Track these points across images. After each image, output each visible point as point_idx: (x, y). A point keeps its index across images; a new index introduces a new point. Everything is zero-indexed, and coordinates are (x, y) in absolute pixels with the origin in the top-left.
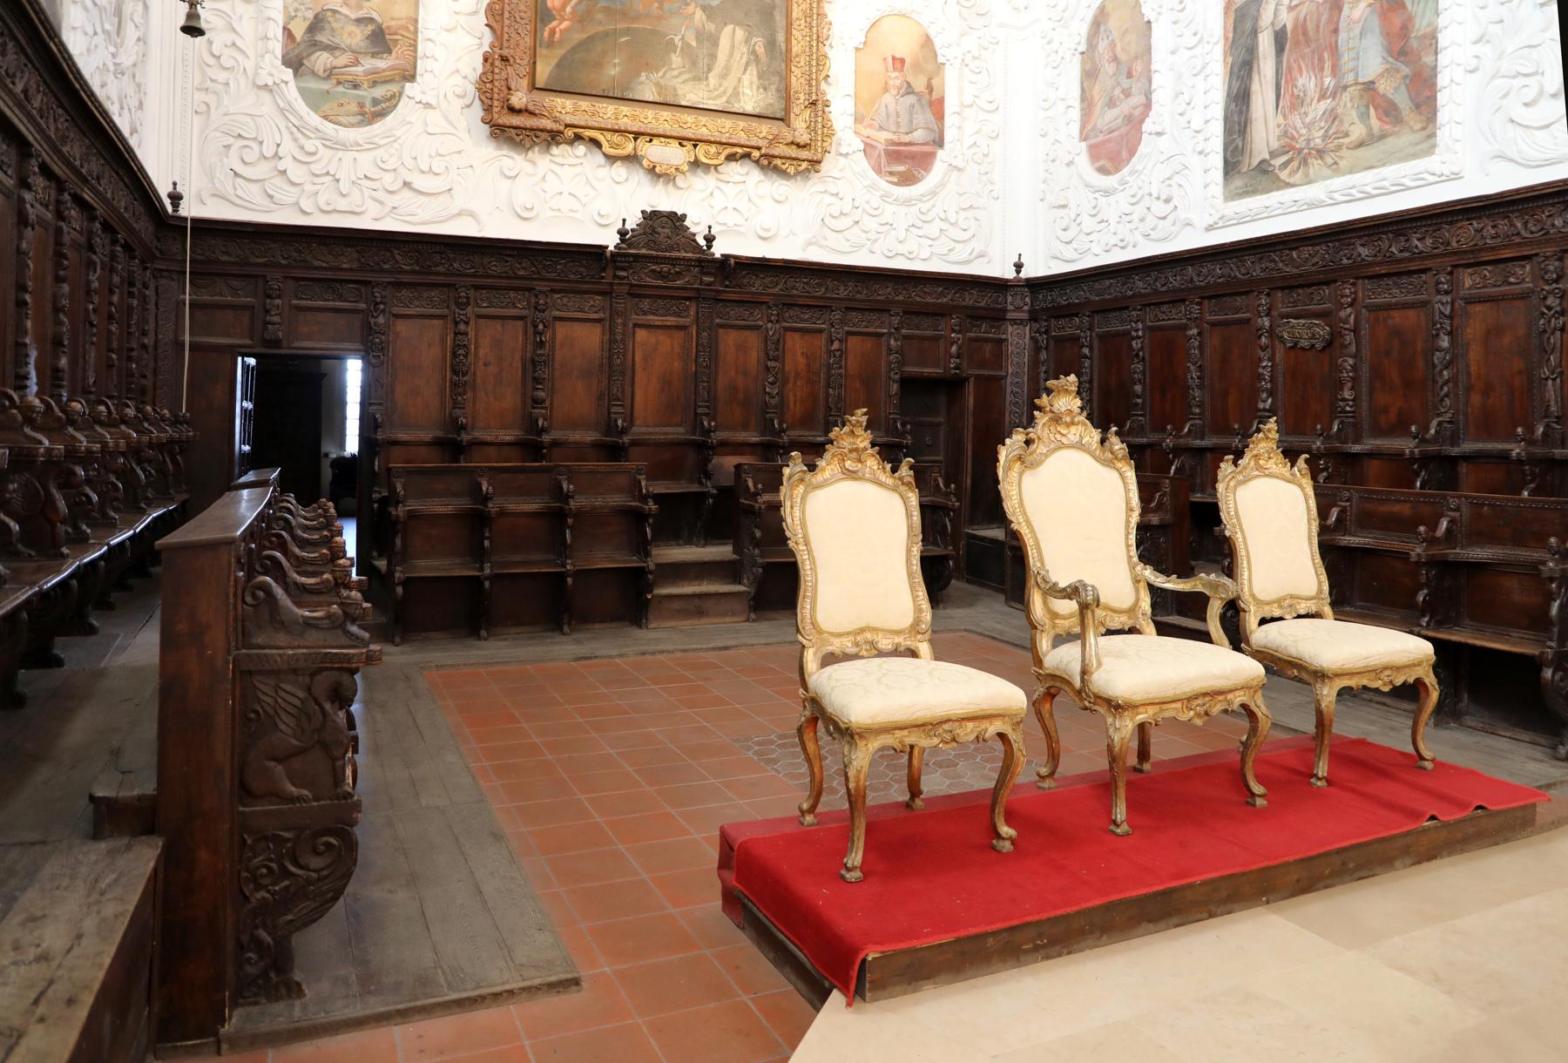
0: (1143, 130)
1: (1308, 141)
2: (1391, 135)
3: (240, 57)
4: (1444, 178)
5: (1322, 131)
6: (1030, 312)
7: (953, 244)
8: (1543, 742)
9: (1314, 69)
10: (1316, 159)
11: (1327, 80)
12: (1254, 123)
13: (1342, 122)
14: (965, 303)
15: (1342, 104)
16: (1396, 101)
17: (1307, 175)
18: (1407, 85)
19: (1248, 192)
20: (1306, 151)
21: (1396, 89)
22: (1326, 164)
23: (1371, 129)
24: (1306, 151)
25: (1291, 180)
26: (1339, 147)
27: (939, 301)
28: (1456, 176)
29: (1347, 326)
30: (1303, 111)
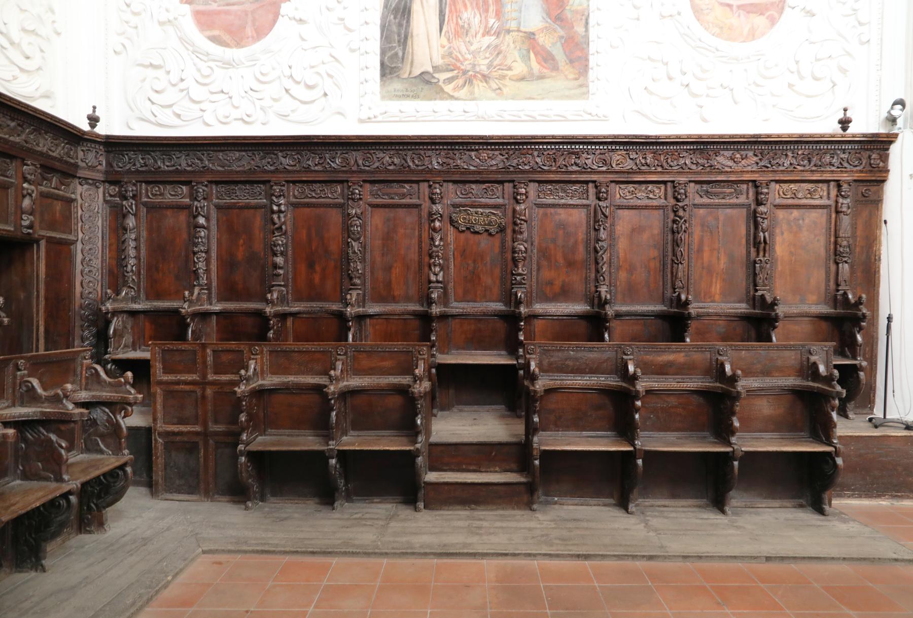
0: (282, 11)
1: (474, 66)
2: (548, 78)
4: (596, 118)
5: (488, 61)
6: (106, 173)
7: (17, 72)
8: (788, 505)
9: (478, 9)
10: (482, 81)
11: (492, 21)
12: (415, 38)
13: (505, 57)
14: (39, 149)
15: (506, 44)
16: (554, 53)
17: (472, 93)
18: (562, 43)
19: (408, 96)
20: (471, 73)
21: (554, 44)
22: (490, 87)
23: (532, 69)
24: (471, 73)
25: (456, 94)
26: (503, 77)
27: (12, 138)
28: (605, 119)
29: (523, 218)
30: (467, 39)
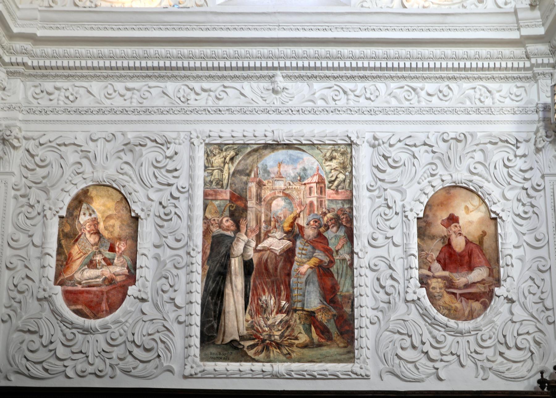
3: (30, 283)
